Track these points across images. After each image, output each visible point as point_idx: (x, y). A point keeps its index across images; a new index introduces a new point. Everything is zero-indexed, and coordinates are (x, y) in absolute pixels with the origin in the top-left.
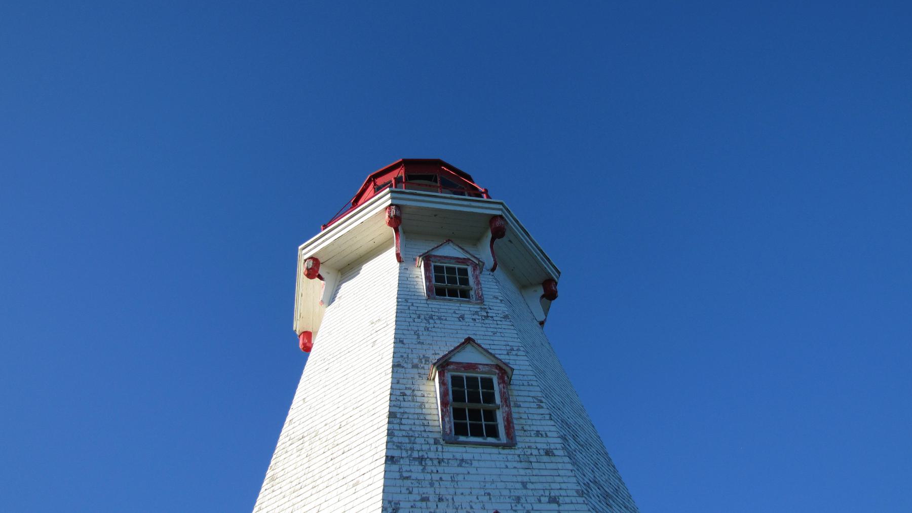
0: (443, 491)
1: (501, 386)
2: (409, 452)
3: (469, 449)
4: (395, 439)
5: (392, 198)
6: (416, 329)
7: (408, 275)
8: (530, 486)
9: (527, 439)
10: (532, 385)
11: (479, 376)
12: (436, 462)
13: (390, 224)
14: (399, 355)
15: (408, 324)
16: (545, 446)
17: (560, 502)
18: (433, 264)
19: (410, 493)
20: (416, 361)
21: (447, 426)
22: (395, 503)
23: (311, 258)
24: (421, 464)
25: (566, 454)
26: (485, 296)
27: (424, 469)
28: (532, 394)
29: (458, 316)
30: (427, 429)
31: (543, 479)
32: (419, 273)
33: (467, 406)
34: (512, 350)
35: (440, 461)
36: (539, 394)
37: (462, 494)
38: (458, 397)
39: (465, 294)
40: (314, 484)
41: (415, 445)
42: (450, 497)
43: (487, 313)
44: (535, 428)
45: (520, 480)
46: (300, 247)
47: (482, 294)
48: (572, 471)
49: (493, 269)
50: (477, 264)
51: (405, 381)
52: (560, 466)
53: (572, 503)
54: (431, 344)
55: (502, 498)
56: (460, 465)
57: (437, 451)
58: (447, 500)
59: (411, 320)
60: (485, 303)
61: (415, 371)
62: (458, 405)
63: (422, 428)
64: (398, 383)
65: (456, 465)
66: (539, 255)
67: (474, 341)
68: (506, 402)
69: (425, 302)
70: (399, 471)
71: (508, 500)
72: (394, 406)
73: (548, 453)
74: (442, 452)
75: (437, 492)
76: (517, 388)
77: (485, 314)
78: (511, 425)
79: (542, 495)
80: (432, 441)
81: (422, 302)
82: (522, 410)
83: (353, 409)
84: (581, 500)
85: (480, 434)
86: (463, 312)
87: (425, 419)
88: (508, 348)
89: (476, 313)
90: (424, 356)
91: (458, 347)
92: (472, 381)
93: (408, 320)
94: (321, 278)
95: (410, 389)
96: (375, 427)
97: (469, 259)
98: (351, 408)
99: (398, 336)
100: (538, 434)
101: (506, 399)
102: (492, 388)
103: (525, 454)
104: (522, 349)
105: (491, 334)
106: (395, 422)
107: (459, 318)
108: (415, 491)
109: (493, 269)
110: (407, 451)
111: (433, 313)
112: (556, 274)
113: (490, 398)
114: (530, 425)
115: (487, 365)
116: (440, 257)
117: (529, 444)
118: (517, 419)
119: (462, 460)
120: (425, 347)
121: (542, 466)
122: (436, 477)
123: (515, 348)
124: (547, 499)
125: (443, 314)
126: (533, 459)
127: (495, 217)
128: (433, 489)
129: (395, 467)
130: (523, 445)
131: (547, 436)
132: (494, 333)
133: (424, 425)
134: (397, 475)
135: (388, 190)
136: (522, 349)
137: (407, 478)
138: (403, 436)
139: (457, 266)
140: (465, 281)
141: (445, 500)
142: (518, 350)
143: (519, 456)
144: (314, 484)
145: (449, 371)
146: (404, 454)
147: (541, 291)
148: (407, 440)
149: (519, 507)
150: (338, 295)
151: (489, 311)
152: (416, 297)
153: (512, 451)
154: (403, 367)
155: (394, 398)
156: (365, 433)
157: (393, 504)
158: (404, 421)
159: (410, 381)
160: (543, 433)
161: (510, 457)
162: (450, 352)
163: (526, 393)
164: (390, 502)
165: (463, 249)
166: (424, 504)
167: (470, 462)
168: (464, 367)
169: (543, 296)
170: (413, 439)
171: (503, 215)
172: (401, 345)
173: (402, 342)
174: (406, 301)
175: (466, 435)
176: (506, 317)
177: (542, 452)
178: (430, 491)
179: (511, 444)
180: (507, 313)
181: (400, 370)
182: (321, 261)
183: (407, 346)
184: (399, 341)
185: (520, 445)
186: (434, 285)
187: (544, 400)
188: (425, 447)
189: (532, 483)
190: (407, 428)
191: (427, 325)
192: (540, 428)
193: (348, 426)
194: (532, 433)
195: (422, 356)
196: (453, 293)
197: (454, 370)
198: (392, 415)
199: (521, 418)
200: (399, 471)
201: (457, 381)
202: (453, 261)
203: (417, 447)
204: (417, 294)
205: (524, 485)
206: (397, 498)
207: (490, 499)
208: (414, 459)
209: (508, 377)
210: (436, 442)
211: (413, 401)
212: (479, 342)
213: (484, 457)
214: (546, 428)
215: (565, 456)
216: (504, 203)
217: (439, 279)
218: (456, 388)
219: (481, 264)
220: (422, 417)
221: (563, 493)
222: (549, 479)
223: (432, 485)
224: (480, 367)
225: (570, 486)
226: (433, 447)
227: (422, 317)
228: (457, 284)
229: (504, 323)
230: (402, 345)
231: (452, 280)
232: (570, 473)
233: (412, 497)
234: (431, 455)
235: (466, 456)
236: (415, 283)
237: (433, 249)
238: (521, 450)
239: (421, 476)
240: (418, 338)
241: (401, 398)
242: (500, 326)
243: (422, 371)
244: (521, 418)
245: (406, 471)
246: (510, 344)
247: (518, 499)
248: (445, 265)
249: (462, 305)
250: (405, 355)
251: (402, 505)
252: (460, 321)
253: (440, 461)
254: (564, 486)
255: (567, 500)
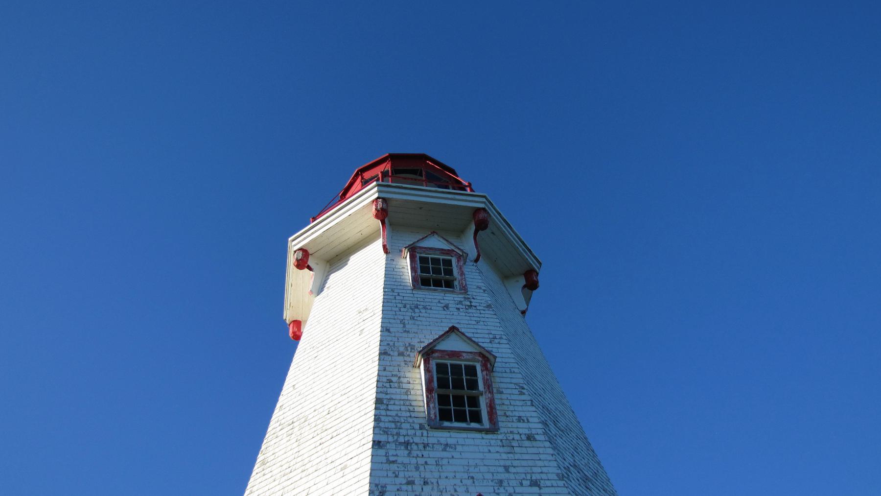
0: (428, 475)
1: (485, 373)
2: (396, 437)
3: (453, 434)
4: (382, 425)
5: (379, 191)
6: (402, 318)
7: (393, 266)
8: (512, 470)
9: (509, 425)
10: (514, 372)
11: (463, 363)
12: (421, 447)
13: (377, 216)
14: (385, 343)
15: (394, 313)
16: (527, 432)
17: (541, 485)
18: (418, 255)
19: (396, 476)
20: (402, 349)
21: (432, 412)
22: (382, 487)
23: (300, 249)
24: (406, 448)
25: (547, 439)
26: (469, 286)
27: (410, 453)
28: (514, 381)
29: (442, 305)
30: (413, 415)
31: (524, 463)
32: (405, 264)
33: (451, 392)
34: (495, 338)
35: (425, 446)
36: (521, 381)
37: (447, 477)
38: (442, 384)
39: (449, 284)
40: (303, 468)
41: (401, 431)
42: (434, 481)
43: (471, 302)
44: (517, 414)
45: (502, 464)
46: (290, 239)
47: (466, 285)
48: (552, 455)
49: (476, 261)
50: (461, 256)
51: (391, 369)
52: (541, 450)
53: (552, 486)
54: (417, 333)
55: (485, 481)
56: (444, 450)
57: (422, 436)
58: (432, 483)
59: (397, 309)
60: (469, 293)
61: (401, 358)
62: (443, 391)
63: (408, 414)
64: (385, 370)
65: (441, 449)
66: (521, 246)
67: (458, 330)
68: (489, 389)
69: (411, 291)
70: (386, 456)
71: (491, 483)
72: (381, 392)
73: (530, 438)
74: (428, 437)
75: (423, 476)
76: (500, 375)
77: (469, 304)
78: (494, 410)
79: (524, 479)
80: (417, 427)
81: (408, 292)
82: (504, 396)
83: (342, 395)
84: (561, 483)
85: (464, 420)
86: (447, 302)
87: (411, 405)
88: (491, 336)
89: (460, 302)
90: (409, 344)
91: (443, 335)
92: (456, 369)
93: (394, 309)
94: (310, 268)
95: (396, 376)
96: (363, 413)
97: (453, 251)
98: (339, 395)
99: (385, 325)
100: (520, 419)
101: (489, 386)
102: (476, 375)
103: (507, 439)
104: (504, 337)
105: (474, 323)
106: (382, 408)
107: (443, 307)
108: (401, 474)
109: (476, 261)
110: (393, 436)
111: (419, 303)
112: (538, 264)
113: (473, 385)
114: (512, 411)
115: (471, 353)
116: (425, 248)
117: (512, 430)
118: (500, 405)
119: (447, 445)
120: (411, 335)
121: (524, 450)
122: (421, 461)
123: (498, 337)
124: (528, 483)
125: (427, 304)
126: (515, 444)
127: (478, 210)
128: (418, 473)
129: (382, 452)
130: (505, 430)
131: (528, 421)
132: (478, 322)
133: (410, 411)
134: (384, 459)
135: (375, 183)
136: (504, 337)
137: (393, 462)
138: (390, 422)
139: (441, 257)
140: (450, 272)
141: (430, 483)
142: (501, 338)
143: (501, 440)
144: (303, 468)
145: (434, 358)
146: (391, 439)
147: (522, 281)
148: (393, 425)
149: (502, 490)
150: (327, 285)
151: (472, 300)
152: (401, 287)
153: (495, 436)
154: (389, 355)
155: (380, 385)
156: (352, 419)
157: (379, 487)
158: (390, 407)
159: (396, 368)
160: (525, 419)
161: (493, 442)
162: (435, 341)
163: (508, 380)
164: (377, 485)
165: (447, 241)
166: (410, 487)
167: (454, 447)
168: (448, 355)
169: (525, 286)
170: (399, 424)
171: (487, 208)
172: (388, 334)
173: (388, 330)
174: (393, 291)
175: (450, 420)
176: (489, 306)
177: (523, 437)
178: (416, 474)
179: (494, 429)
180: (490, 302)
181: (386, 357)
182: (310, 252)
183: (393, 334)
184: (385, 330)
185: (502, 430)
186: (420, 275)
187: (525, 387)
188: (411, 432)
189: (514, 467)
190: (394, 413)
191: (413, 315)
192: (522, 414)
193: (336, 412)
194: (514, 419)
195: (407, 345)
196: (438, 284)
197: (438, 358)
198: (378, 401)
199: (503, 404)
200: (386, 456)
201: (441, 368)
202: (438, 252)
203: (403, 432)
204: (403, 284)
205: (507, 469)
206: (383, 481)
207: (474, 482)
208: (401, 443)
209: (491, 364)
210: (422, 427)
211: (399, 387)
212: (463, 330)
213: (468, 442)
214: (528, 414)
215: (546, 441)
216: (487, 196)
217: (424, 270)
218: (440, 376)
219: (465, 255)
220: (407, 403)
221: (544, 476)
222: (530, 463)
223: (417, 468)
224: (464, 354)
225: (551, 470)
226: (419, 432)
227: (408, 306)
228: (441, 274)
229: (487, 312)
230: (388, 334)
231: (437, 271)
232: (550, 458)
233: (398, 481)
234: (417, 440)
235: (451, 441)
236: (401, 274)
237: (418, 241)
238: (503, 435)
239: (406, 460)
240: (404, 326)
241: (388, 385)
242: (483, 316)
243: (407, 359)
244: (503, 404)
245: (393, 455)
246: (493, 332)
247: (501, 482)
248: (430, 256)
249: (446, 295)
250: (391, 343)
251: (389, 488)
252: (444, 310)
253: (425, 446)
254: (545, 470)
255: (548, 483)
